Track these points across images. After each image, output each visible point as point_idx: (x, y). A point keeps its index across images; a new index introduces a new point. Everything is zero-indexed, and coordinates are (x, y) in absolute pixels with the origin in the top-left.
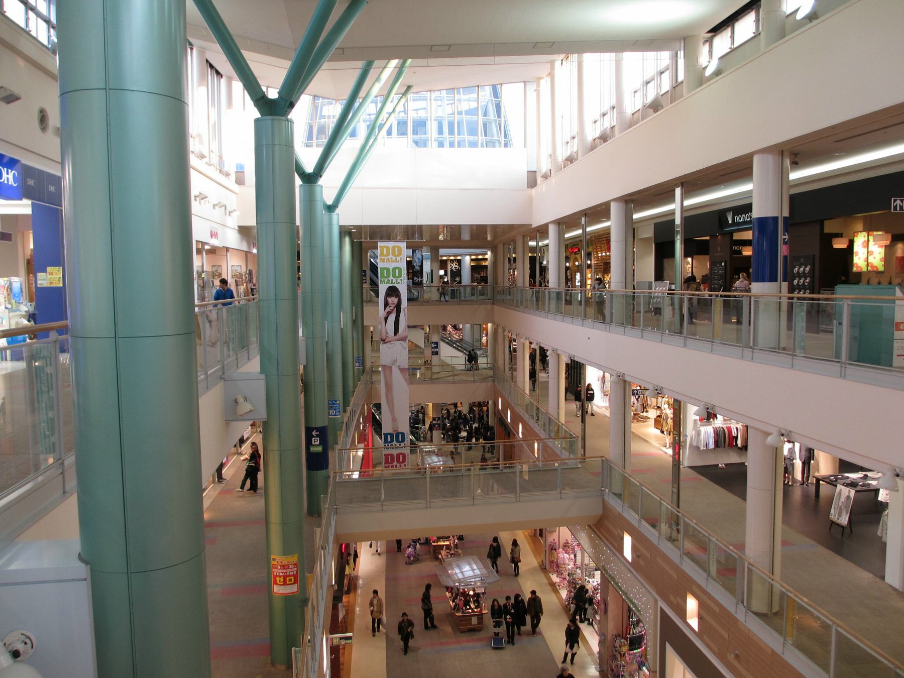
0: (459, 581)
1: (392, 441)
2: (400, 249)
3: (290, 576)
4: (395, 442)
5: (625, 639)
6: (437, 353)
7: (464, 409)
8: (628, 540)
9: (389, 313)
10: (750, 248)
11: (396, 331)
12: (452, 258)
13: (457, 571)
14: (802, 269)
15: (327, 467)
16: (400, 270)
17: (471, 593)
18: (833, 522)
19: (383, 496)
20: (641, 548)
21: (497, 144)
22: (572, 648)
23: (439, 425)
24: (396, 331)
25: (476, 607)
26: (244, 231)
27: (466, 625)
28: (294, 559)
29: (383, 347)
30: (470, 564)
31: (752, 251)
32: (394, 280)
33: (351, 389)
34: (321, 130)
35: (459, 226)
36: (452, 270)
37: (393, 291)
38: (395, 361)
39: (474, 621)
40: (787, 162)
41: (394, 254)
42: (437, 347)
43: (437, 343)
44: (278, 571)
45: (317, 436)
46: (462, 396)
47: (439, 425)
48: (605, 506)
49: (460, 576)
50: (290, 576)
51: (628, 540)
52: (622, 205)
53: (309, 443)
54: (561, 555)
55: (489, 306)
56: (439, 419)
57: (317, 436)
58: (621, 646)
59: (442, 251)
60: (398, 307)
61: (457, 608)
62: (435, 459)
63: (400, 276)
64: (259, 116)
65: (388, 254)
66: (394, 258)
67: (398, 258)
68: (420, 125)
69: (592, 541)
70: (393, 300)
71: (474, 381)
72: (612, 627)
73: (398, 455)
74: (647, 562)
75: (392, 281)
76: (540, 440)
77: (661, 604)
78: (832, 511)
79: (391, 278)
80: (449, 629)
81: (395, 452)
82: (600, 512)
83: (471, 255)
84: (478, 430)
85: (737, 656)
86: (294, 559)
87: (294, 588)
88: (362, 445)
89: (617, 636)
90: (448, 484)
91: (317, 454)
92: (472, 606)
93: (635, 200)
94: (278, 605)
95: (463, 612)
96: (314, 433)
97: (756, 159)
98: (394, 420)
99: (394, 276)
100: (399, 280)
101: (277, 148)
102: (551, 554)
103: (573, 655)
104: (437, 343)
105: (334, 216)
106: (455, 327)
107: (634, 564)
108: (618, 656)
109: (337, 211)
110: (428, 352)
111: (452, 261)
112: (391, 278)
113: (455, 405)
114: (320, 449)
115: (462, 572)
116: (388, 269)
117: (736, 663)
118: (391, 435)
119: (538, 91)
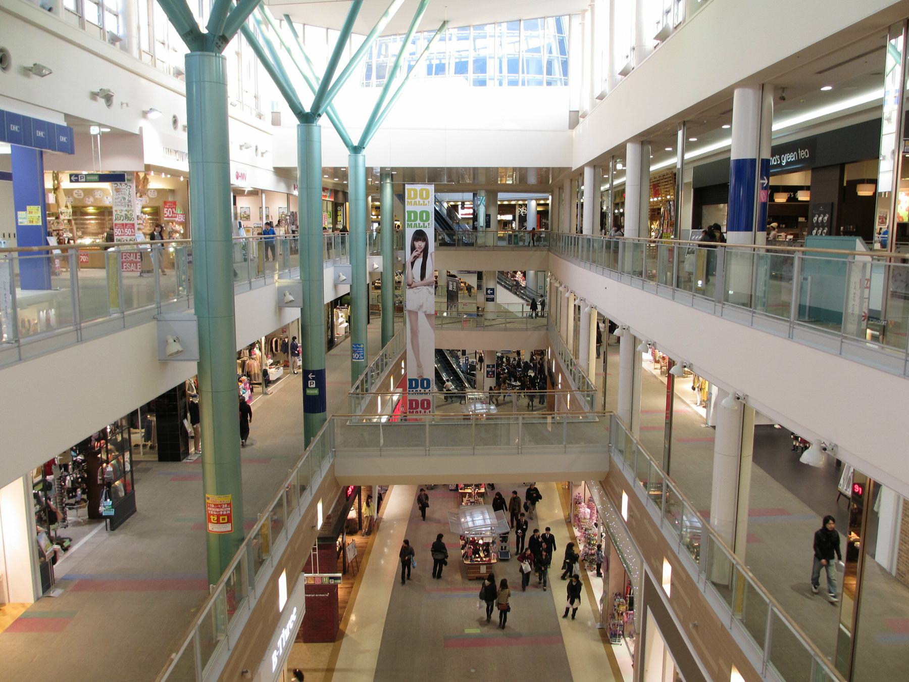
0: (469, 529)
1: (417, 386)
2: (427, 191)
3: (223, 515)
4: (419, 388)
5: (625, 598)
6: (493, 300)
7: (526, 357)
8: (625, 498)
9: (416, 258)
10: (808, 193)
11: (423, 276)
12: (521, 202)
13: (469, 519)
14: (820, 218)
15: (324, 410)
16: (427, 213)
17: (481, 542)
18: (841, 493)
19: (382, 441)
20: (634, 508)
21: (559, 83)
22: (572, 603)
23: (493, 372)
24: (423, 276)
25: (485, 556)
26: (282, 173)
27: (473, 573)
28: (228, 498)
29: (409, 293)
30: (483, 514)
31: (770, 196)
32: (422, 224)
33: (390, 333)
34: (380, 67)
35: (526, 169)
36: (520, 215)
37: (420, 235)
38: (421, 306)
39: (483, 569)
40: (770, 100)
41: (421, 197)
42: (493, 294)
43: (493, 290)
44: (212, 510)
45: (313, 379)
46: (522, 344)
47: (493, 372)
48: (611, 463)
49: (470, 524)
50: (223, 515)
51: (625, 498)
52: (637, 147)
53: (305, 386)
54: (582, 510)
55: (544, 253)
56: (493, 366)
57: (313, 379)
58: (619, 606)
59: (501, 195)
60: (425, 251)
61: (466, 556)
62: (479, 406)
63: (428, 219)
64: (189, 52)
65: (415, 197)
66: (421, 202)
67: (426, 202)
68: (481, 65)
69: (601, 497)
70: (420, 244)
71: (527, 329)
72: (613, 587)
73: (423, 401)
74: (638, 525)
75: (419, 225)
76: (571, 391)
77: (646, 567)
78: (841, 481)
79: (418, 221)
80: (458, 577)
81: (419, 398)
82: (606, 469)
83: (536, 200)
84: (529, 378)
85: (695, 626)
86: (228, 498)
87: (228, 527)
88: (400, 390)
89: (618, 595)
90: (487, 433)
91: (313, 397)
92: (482, 555)
93: (655, 140)
94: (214, 542)
95: (471, 560)
96: (310, 376)
97: (737, 93)
98: (419, 366)
99: (421, 219)
100: (426, 224)
101: (207, 85)
102: (576, 508)
103: (575, 610)
104: (493, 290)
105: (360, 157)
106: (524, 274)
107: (628, 523)
108: (616, 614)
109: (364, 152)
110: (481, 297)
111: (521, 206)
112: (418, 221)
113: (518, 353)
114: (316, 392)
115: (473, 521)
116: (415, 213)
117: (694, 632)
118: (416, 381)
119: (582, 24)
